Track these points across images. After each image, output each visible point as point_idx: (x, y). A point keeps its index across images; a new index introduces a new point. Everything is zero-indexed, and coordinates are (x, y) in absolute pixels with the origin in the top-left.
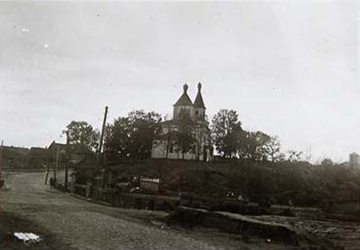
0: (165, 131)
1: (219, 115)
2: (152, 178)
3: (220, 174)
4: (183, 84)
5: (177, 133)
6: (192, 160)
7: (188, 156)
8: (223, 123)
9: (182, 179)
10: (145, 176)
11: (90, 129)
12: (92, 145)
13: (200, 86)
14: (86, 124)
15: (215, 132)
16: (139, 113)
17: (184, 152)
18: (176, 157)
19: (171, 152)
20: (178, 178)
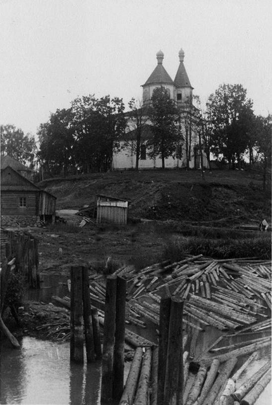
0: (131, 126)
1: (218, 93)
2: (116, 200)
3: (226, 186)
4: (157, 51)
5: (151, 126)
6: (177, 169)
7: (171, 162)
8: (225, 106)
9: (165, 199)
10: (105, 198)
11: (19, 134)
12: (26, 157)
13: (182, 55)
14: (212, 95)
15: (213, 122)
16: (86, 100)
17: (164, 156)
18: (152, 166)
19: (144, 158)
20: (157, 197)
